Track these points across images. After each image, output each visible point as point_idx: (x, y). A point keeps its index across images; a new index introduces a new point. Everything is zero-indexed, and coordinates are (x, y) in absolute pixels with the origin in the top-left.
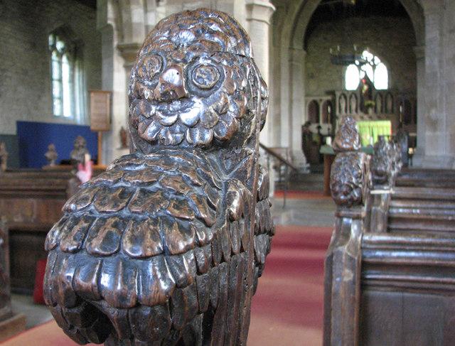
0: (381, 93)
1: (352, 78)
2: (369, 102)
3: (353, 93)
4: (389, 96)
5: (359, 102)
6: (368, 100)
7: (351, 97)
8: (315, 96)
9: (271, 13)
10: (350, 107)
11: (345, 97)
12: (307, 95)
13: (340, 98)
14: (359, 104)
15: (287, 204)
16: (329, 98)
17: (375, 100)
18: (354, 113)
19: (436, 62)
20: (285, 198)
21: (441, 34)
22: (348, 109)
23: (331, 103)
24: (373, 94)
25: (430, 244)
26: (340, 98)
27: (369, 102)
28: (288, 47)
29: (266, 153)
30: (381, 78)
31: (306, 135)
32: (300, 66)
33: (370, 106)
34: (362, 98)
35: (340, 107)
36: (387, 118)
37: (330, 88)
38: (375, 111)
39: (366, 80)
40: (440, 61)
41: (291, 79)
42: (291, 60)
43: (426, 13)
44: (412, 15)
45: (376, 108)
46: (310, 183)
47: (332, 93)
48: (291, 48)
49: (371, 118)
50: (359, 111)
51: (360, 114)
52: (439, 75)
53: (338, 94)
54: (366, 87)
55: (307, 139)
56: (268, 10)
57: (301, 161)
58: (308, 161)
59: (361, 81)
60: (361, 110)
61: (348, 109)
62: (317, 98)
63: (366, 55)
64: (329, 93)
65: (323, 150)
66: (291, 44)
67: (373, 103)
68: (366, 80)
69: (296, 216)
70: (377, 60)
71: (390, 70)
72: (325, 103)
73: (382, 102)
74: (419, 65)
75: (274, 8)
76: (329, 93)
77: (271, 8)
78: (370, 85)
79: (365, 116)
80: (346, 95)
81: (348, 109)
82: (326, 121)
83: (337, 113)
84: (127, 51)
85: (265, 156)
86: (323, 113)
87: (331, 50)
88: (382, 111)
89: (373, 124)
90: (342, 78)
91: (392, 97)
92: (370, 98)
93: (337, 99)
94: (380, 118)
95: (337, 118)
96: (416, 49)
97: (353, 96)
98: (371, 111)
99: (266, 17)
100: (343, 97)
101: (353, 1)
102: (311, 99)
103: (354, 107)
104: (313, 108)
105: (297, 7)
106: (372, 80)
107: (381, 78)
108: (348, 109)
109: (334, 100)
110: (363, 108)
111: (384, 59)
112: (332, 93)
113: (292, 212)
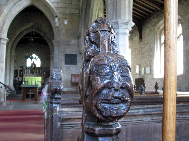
0: (38, 68)
1: (29, 63)
2: (34, 71)
3: (29, 68)
4: (41, 69)
5: (31, 70)
6: (34, 70)
7: (28, 69)
8: (16, 68)
9: (7, 41)
10: (28, 72)
11: (27, 69)
12: (14, 68)
13: (25, 69)
14: (31, 71)
15: (11, 103)
16: (21, 69)
17: (36, 70)
18: (29, 74)
19: (57, 60)
20: (10, 101)
21: (59, 53)
22: (27, 73)
23: (22, 71)
24: (36, 68)
25: (66, 100)
26: (25, 69)
27: (34, 71)
28: (10, 52)
29: (4, 87)
30: (38, 63)
31: (15, 81)
32: (13, 58)
33: (34, 72)
34: (32, 69)
35: (25, 72)
36: (40, 76)
37: (21, 66)
38: (36, 74)
39: (33, 64)
40: (58, 60)
41: (10, 62)
42: (11, 56)
43: (54, 46)
44: (50, 45)
45: (36, 73)
46: (16, 97)
47: (22, 67)
48: (11, 52)
49: (35, 76)
50: (31, 73)
51: (31, 74)
52: (58, 64)
53: (24, 68)
54: (34, 66)
55: (15, 82)
56: (6, 41)
57: (13, 88)
58: (15, 90)
59: (32, 64)
60: (32, 73)
61: (27, 73)
62: (17, 69)
63: (34, 55)
64: (21, 67)
65: (22, 86)
66: (11, 51)
67: (36, 71)
68: (33, 64)
69: (14, 107)
70: (37, 57)
71: (41, 61)
72: (19, 71)
73: (38, 71)
74: (51, 60)
75: (8, 40)
76: (21, 67)
77: (7, 40)
78: (35, 65)
79: (33, 75)
80: (27, 68)
81: (27, 72)
82: (20, 76)
83: (24, 74)
85: (4, 87)
86: (19, 73)
87: (25, 54)
88: (38, 74)
89: (36, 78)
90: (26, 63)
92: (35, 69)
93: (24, 69)
94: (38, 76)
95: (24, 76)
96: (50, 55)
97: (29, 69)
98: (35, 74)
99: (5, 42)
100: (26, 69)
101: (100, 139)
102: (15, 69)
103: (29, 72)
104: (16, 72)
105: (14, 39)
106: (35, 64)
107: (38, 63)
108: (27, 72)
109: (23, 70)
110: (33, 73)
111: (40, 57)
112: (22, 67)
113: (13, 105)
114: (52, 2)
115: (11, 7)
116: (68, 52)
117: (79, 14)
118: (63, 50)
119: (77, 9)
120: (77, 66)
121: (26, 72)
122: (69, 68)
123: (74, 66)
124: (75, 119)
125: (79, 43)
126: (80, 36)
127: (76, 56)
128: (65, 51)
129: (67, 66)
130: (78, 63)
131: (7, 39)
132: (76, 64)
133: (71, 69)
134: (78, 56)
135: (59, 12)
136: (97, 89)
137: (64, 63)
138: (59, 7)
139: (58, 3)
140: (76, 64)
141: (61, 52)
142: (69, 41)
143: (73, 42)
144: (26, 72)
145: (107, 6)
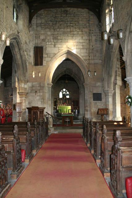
6: (65, 101)
40: (88, 98)
53: (58, 99)
84: (20, 94)
91: (70, 100)
94: (68, 105)
114: (82, 56)
115: (79, 85)
116: (95, 92)
117: (102, 63)
118: (92, 91)
119: (100, 60)
120: (102, 101)
121: (59, 102)
122: (96, 103)
123: (100, 101)
124: (126, 152)
125: (102, 85)
126: (103, 80)
127: (101, 94)
128: (93, 91)
129: (95, 101)
130: (102, 99)
131: (52, 84)
132: (101, 100)
133: (98, 104)
134: (102, 94)
135: (87, 63)
136: (57, 42)
137: (93, 99)
138: (87, 59)
139: (81, 49)
140: (101, 100)
141: (90, 92)
142: (95, 84)
143: (99, 84)
144: (59, 102)
145: (126, 67)
